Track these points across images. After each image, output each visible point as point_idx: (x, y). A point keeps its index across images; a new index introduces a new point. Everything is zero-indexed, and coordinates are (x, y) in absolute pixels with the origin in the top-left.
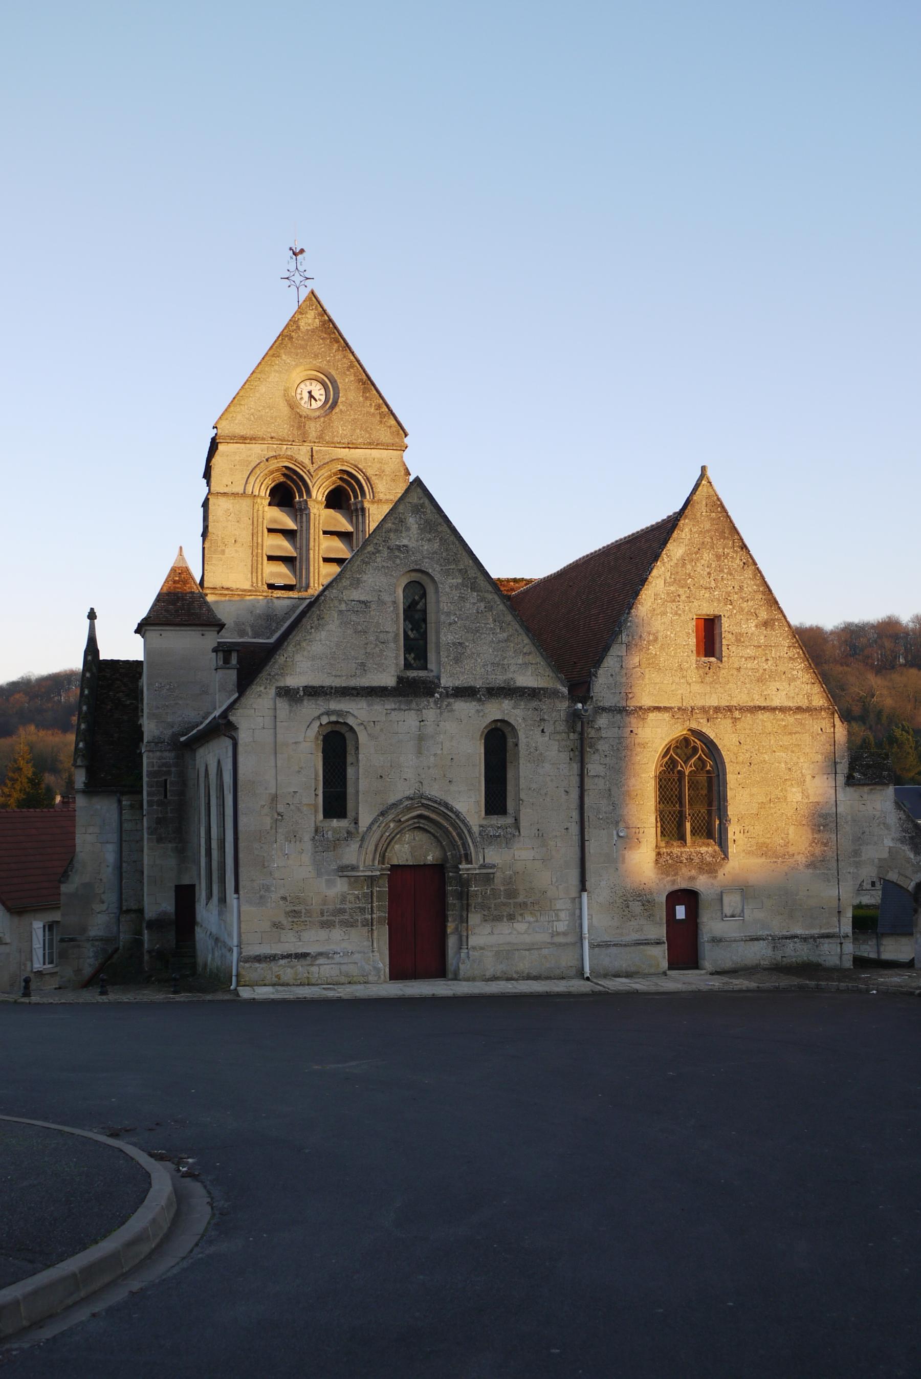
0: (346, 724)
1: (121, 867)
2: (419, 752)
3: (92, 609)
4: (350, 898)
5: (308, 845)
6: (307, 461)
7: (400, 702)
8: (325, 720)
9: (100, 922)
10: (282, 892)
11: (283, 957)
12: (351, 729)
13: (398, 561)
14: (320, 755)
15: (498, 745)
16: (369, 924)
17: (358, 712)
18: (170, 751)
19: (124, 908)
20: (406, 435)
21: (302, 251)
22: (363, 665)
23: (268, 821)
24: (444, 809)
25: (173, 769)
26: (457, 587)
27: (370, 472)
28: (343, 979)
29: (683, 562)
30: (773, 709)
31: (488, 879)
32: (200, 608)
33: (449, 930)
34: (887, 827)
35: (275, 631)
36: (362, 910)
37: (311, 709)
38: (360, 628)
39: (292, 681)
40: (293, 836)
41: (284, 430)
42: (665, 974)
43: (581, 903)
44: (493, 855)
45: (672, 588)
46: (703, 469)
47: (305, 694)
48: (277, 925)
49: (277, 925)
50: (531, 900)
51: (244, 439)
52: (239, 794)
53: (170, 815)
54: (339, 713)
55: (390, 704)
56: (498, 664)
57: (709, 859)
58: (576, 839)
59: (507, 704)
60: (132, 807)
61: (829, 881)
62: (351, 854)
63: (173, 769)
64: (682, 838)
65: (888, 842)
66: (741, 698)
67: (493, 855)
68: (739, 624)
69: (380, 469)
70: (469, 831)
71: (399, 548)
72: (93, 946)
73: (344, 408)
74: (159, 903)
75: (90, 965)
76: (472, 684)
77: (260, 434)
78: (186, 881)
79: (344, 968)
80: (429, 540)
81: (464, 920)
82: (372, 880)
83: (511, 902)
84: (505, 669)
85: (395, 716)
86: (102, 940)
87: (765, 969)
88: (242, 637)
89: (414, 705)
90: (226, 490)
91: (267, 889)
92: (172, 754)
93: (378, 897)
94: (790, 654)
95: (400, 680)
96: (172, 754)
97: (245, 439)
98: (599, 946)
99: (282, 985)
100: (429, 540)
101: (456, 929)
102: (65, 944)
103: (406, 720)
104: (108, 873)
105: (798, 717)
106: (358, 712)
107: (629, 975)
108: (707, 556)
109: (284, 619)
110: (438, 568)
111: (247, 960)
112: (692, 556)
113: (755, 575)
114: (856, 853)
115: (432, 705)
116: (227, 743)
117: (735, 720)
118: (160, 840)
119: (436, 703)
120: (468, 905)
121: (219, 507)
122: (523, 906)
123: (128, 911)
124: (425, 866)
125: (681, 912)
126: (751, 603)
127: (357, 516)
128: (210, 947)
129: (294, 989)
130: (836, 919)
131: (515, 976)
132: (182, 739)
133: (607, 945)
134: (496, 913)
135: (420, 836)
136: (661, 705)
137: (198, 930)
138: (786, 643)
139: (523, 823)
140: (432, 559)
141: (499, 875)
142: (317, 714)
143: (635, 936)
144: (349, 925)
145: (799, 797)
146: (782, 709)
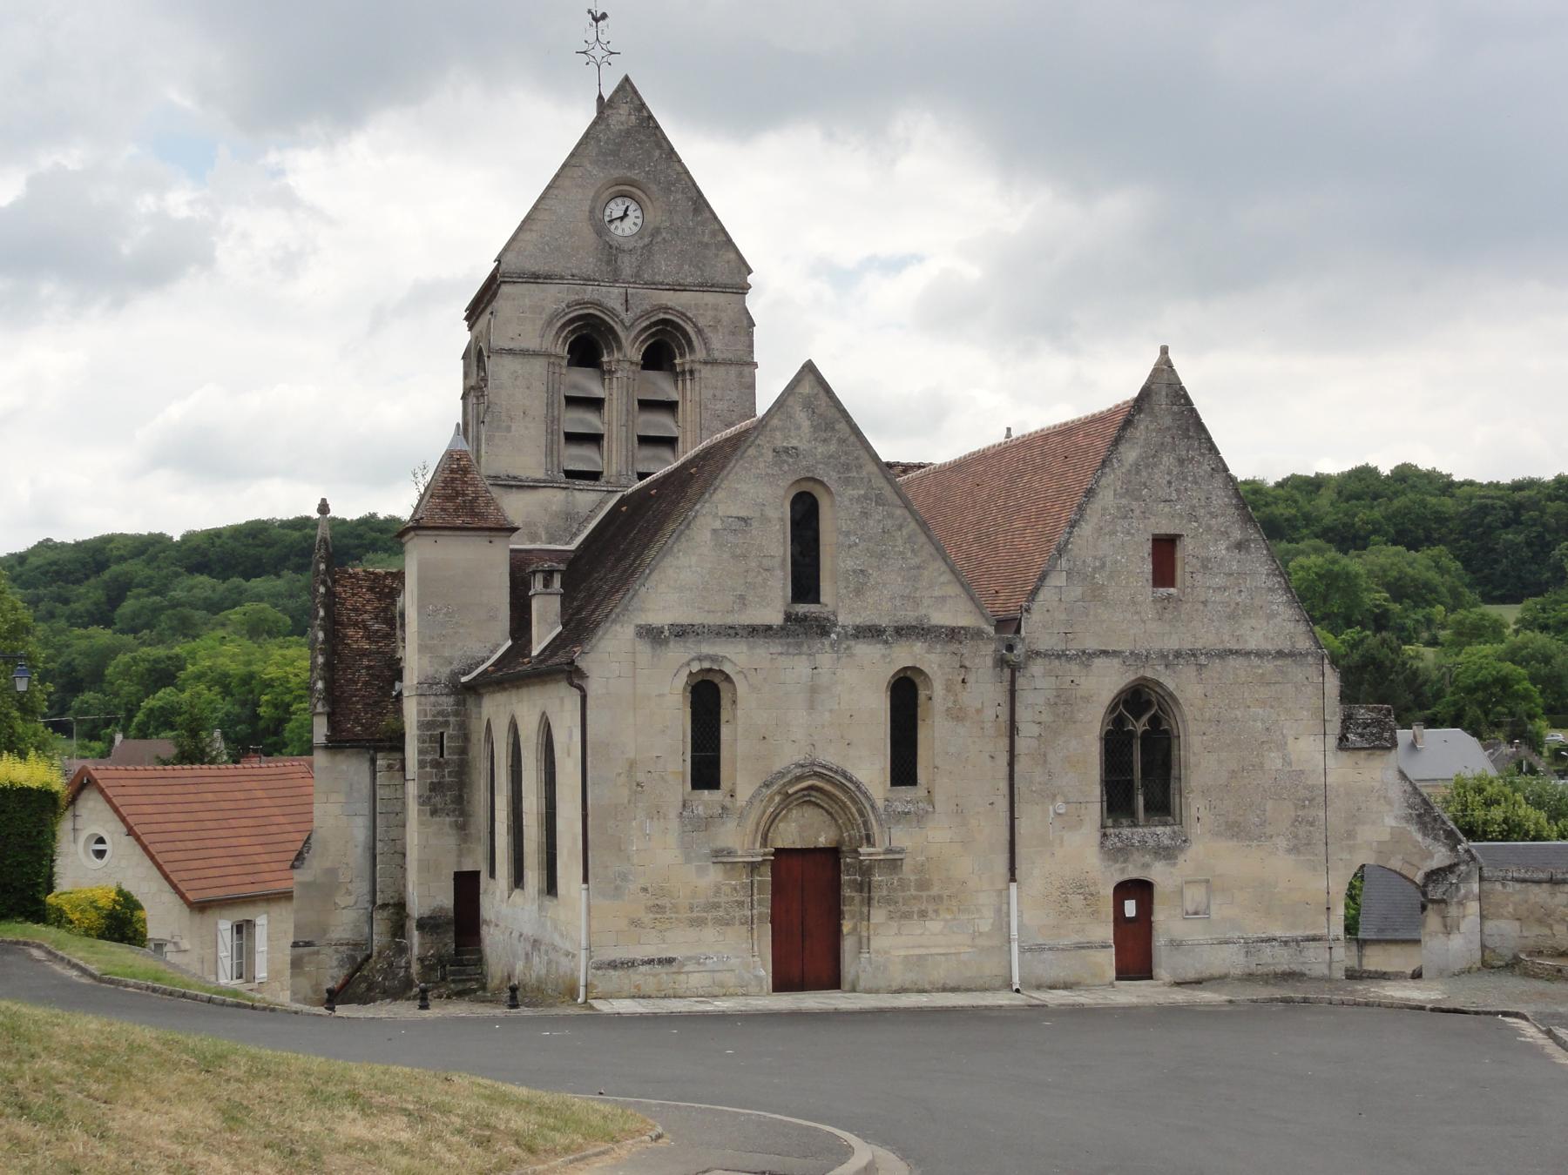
0: (721, 672)
1: (374, 848)
2: (811, 707)
3: (324, 500)
5: (674, 824)
6: (619, 308)
7: (788, 645)
8: (695, 667)
9: (346, 919)
10: (642, 882)
11: (644, 963)
12: (728, 678)
13: (786, 467)
14: (689, 710)
15: (905, 695)
19: (379, 902)
20: (750, 271)
21: (604, 16)
22: (742, 597)
23: (626, 792)
25: (452, 719)
26: (858, 500)
28: (716, 990)
29: (1137, 468)
30: (1248, 654)
31: (894, 865)
32: (487, 504)
34: (1390, 803)
35: (576, 535)
36: (741, 904)
38: (738, 551)
39: (660, 616)
40: (657, 813)
42: (1111, 984)
43: (1008, 896)
44: (901, 837)
45: (1124, 501)
48: (635, 923)
50: (947, 893)
51: (535, 278)
52: (589, 759)
53: (447, 779)
54: (713, 659)
55: (776, 647)
56: (909, 597)
57: (1167, 842)
59: (919, 647)
60: (390, 767)
61: (1315, 869)
63: (452, 719)
64: (1131, 813)
65: (1390, 821)
66: (1206, 637)
67: (901, 837)
68: (1205, 546)
69: (715, 317)
70: (873, 807)
71: (786, 450)
72: (337, 951)
73: (668, 237)
74: (428, 894)
75: (333, 978)
76: (877, 622)
77: (558, 270)
79: (718, 976)
80: (825, 440)
82: (753, 867)
83: (927, 896)
84: (917, 603)
85: (784, 661)
87: (1234, 979)
88: (533, 541)
91: (624, 877)
92: (451, 700)
93: (759, 889)
94: (1269, 584)
95: (788, 617)
96: (451, 700)
97: (538, 277)
98: (1030, 950)
99: (643, 997)
100: (825, 440)
101: (855, 929)
102: (301, 950)
103: (795, 667)
104: (357, 856)
105: (1279, 663)
106: (736, 657)
107: (1067, 986)
108: (1167, 460)
109: (588, 519)
110: (834, 475)
112: (1149, 461)
113: (1226, 485)
114: (1350, 835)
115: (827, 647)
117: (1201, 667)
118: (434, 812)
119: (832, 645)
120: (870, 899)
121: (501, 370)
123: (384, 906)
125: (1130, 908)
126: (1221, 520)
127: (684, 381)
128: (521, 952)
129: (658, 1001)
130: (1323, 918)
131: (927, 987)
132: (464, 679)
133: (1041, 948)
135: (810, 814)
136: (1110, 649)
137: (484, 930)
138: (1264, 570)
139: (939, 798)
140: (827, 464)
143: (1076, 938)
145: (1279, 763)
146: (1260, 654)
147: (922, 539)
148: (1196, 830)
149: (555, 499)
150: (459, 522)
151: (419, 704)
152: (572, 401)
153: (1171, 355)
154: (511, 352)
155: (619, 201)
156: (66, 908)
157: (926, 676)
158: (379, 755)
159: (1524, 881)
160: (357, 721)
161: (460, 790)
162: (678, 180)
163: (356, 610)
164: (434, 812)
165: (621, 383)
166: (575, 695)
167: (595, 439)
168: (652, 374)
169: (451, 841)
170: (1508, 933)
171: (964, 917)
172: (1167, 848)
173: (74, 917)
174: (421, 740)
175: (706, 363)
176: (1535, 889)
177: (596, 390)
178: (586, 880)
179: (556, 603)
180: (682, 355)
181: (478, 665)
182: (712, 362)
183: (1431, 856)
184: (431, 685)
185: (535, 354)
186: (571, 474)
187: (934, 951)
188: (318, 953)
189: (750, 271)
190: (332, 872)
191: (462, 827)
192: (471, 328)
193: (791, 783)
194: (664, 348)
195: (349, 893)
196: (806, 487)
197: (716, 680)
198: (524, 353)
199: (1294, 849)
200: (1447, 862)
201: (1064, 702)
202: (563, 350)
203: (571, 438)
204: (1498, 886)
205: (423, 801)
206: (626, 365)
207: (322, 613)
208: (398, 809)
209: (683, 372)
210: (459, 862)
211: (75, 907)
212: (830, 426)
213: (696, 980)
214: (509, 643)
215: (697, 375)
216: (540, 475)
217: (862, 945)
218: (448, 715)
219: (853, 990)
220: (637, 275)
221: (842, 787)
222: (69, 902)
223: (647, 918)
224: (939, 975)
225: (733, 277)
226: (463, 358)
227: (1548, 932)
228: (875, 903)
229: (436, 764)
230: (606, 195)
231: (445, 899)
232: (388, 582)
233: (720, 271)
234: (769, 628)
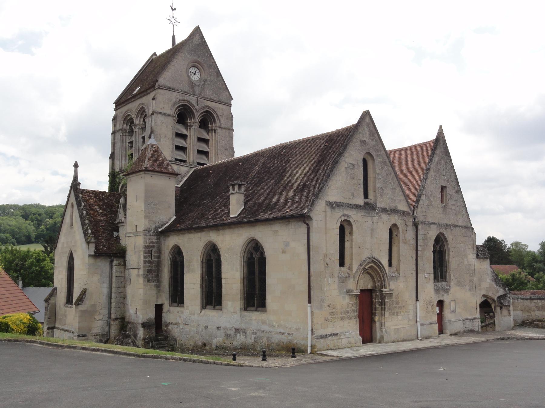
3: (76, 162)
4: (350, 305)
5: (336, 279)
15: (392, 231)
17: (355, 216)
18: (154, 235)
20: (232, 99)
21: (175, 9)
22: (353, 194)
23: (323, 267)
25: (155, 245)
27: (218, 113)
30: (459, 226)
31: (391, 295)
35: (180, 182)
39: (332, 199)
40: (332, 276)
41: (186, 88)
46: (441, 127)
49: (326, 319)
53: (153, 268)
54: (348, 216)
58: (415, 277)
59: (397, 217)
60: (119, 264)
63: (155, 245)
71: (363, 141)
72: (95, 338)
81: (383, 315)
86: (99, 335)
89: (370, 215)
90: (161, 111)
91: (323, 301)
92: (155, 237)
95: (365, 203)
96: (155, 237)
104: (104, 299)
106: (355, 216)
109: (184, 176)
114: (480, 285)
116: (303, 229)
118: (149, 281)
120: (385, 308)
122: (400, 307)
123: (116, 319)
132: (160, 230)
134: (393, 311)
142: (340, 216)
144: (350, 318)
147: (395, 179)
148: (452, 283)
150: (160, 170)
151: (144, 238)
153: (443, 128)
154: (161, 113)
155: (193, 68)
156: (10, 323)
158: (115, 259)
159: (523, 299)
160: (104, 246)
161: (158, 272)
162: (212, 65)
163: (92, 204)
164: (149, 281)
165: (194, 132)
167: (200, 140)
169: (154, 292)
170: (520, 315)
171: (406, 314)
172: (446, 289)
173: (14, 327)
174: (145, 253)
175: (220, 127)
176: (526, 301)
177: (184, 132)
178: (310, 302)
179: (242, 198)
180: (211, 124)
181: (166, 224)
183: (498, 292)
186: (176, 160)
187: (401, 326)
189: (232, 99)
190: (94, 306)
191: (158, 287)
192: (116, 109)
193: (366, 265)
194: (207, 121)
195: (100, 314)
198: (165, 115)
199: (470, 290)
200: (503, 294)
201: (425, 239)
204: (516, 301)
207: (83, 204)
208: (122, 280)
210: (157, 301)
211: (14, 323)
212: (373, 135)
213: (344, 342)
214: (175, 217)
215: (217, 131)
218: (154, 243)
219: (380, 342)
220: (200, 94)
222: (11, 321)
223: (329, 317)
224: (402, 335)
225: (227, 101)
227: (530, 314)
228: (386, 310)
229: (150, 262)
230: (190, 65)
231: (152, 315)
232: (101, 195)
233: (224, 99)
234: (360, 206)
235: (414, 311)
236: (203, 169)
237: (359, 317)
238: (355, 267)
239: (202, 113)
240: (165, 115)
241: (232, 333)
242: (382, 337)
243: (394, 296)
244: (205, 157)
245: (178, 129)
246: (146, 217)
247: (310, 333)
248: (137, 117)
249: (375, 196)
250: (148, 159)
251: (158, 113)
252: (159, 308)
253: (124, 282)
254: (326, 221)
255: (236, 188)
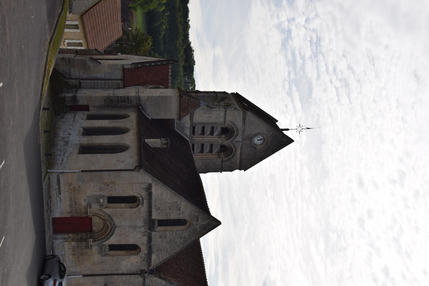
0: (139, 204)
2: (129, 226)
4: (80, 207)
5: (98, 194)
8: (140, 198)
9: (76, 72)
12: (138, 206)
15: (133, 248)
16: (71, 212)
17: (144, 209)
19: (81, 81)
20: (245, 171)
22: (159, 209)
24: (111, 234)
25: (130, 104)
27: (232, 159)
31: (87, 247)
33: (69, 235)
35: (178, 130)
36: (76, 210)
37: (144, 194)
40: (101, 189)
43: (79, 275)
44: (95, 249)
47: (150, 192)
49: (70, 184)
52: (115, 172)
54: (143, 203)
59: (146, 252)
62: (95, 207)
63: (130, 104)
67: (95, 249)
74: (84, 95)
78: (90, 108)
85: (142, 220)
90: (227, 114)
91: (83, 181)
95: (154, 220)
101: (70, 237)
104: (94, 75)
109: (183, 133)
111: (58, 176)
118: (105, 100)
120: (78, 241)
122: (78, 258)
123: (80, 83)
124: (92, 227)
134: (76, 250)
135: (102, 226)
139: (106, 258)
141: (88, 250)
142: (142, 196)
144: (71, 206)
149: (188, 125)
151: (134, 96)
152: (213, 128)
154: (226, 114)
157: (138, 254)
164: (105, 100)
165: (217, 140)
166: (132, 168)
167: (203, 133)
168: (219, 146)
177: (216, 134)
178: (82, 171)
179: (159, 146)
180: (224, 154)
182: (222, 162)
184: (139, 99)
185: (225, 119)
186: (194, 128)
188: (67, 65)
189: (245, 171)
193: (109, 222)
196: (188, 223)
197: (137, 202)
198: (225, 117)
202: (226, 126)
203: (203, 128)
205: (108, 97)
206: (222, 142)
207: (159, 64)
209: (220, 155)
216: (194, 121)
217: (65, 239)
221: (108, 235)
223: (72, 187)
226: (224, 92)
230: (264, 136)
231: (81, 102)
235: (75, 273)
236: (190, 148)
237: (72, 218)
238: (107, 211)
239: (231, 147)
240: (225, 117)
241: (66, 139)
242: (56, 239)
243: (87, 250)
244: (199, 150)
245: (217, 128)
246: (148, 97)
247: (61, 171)
248: (224, 103)
249: (159, 231)
250: (188, 99)
251: (226, 111)
252: (86, 108)
253: (104, 88)
254: (138, 183)
255: (166, 142)
